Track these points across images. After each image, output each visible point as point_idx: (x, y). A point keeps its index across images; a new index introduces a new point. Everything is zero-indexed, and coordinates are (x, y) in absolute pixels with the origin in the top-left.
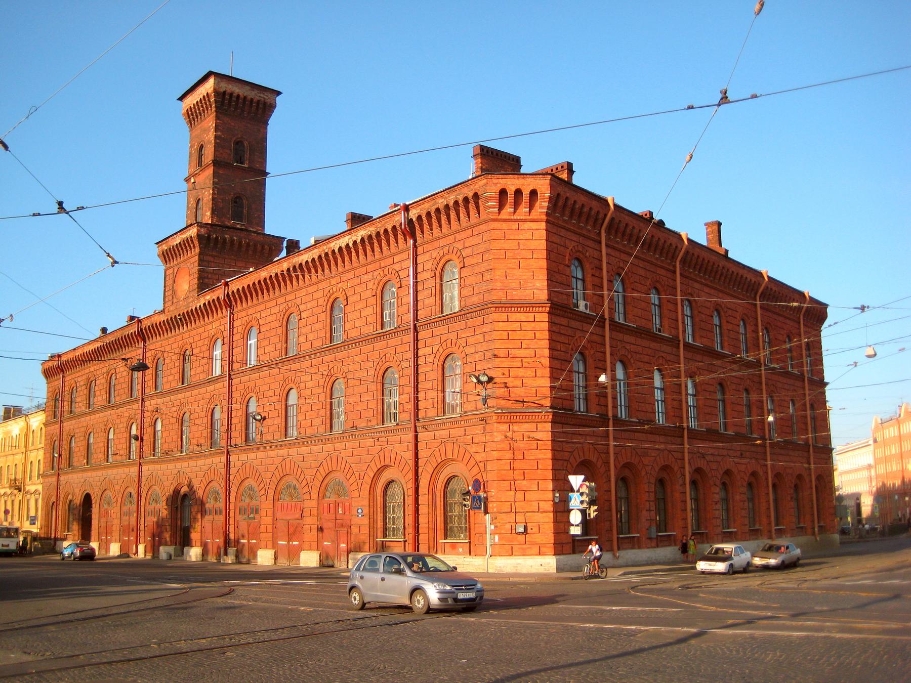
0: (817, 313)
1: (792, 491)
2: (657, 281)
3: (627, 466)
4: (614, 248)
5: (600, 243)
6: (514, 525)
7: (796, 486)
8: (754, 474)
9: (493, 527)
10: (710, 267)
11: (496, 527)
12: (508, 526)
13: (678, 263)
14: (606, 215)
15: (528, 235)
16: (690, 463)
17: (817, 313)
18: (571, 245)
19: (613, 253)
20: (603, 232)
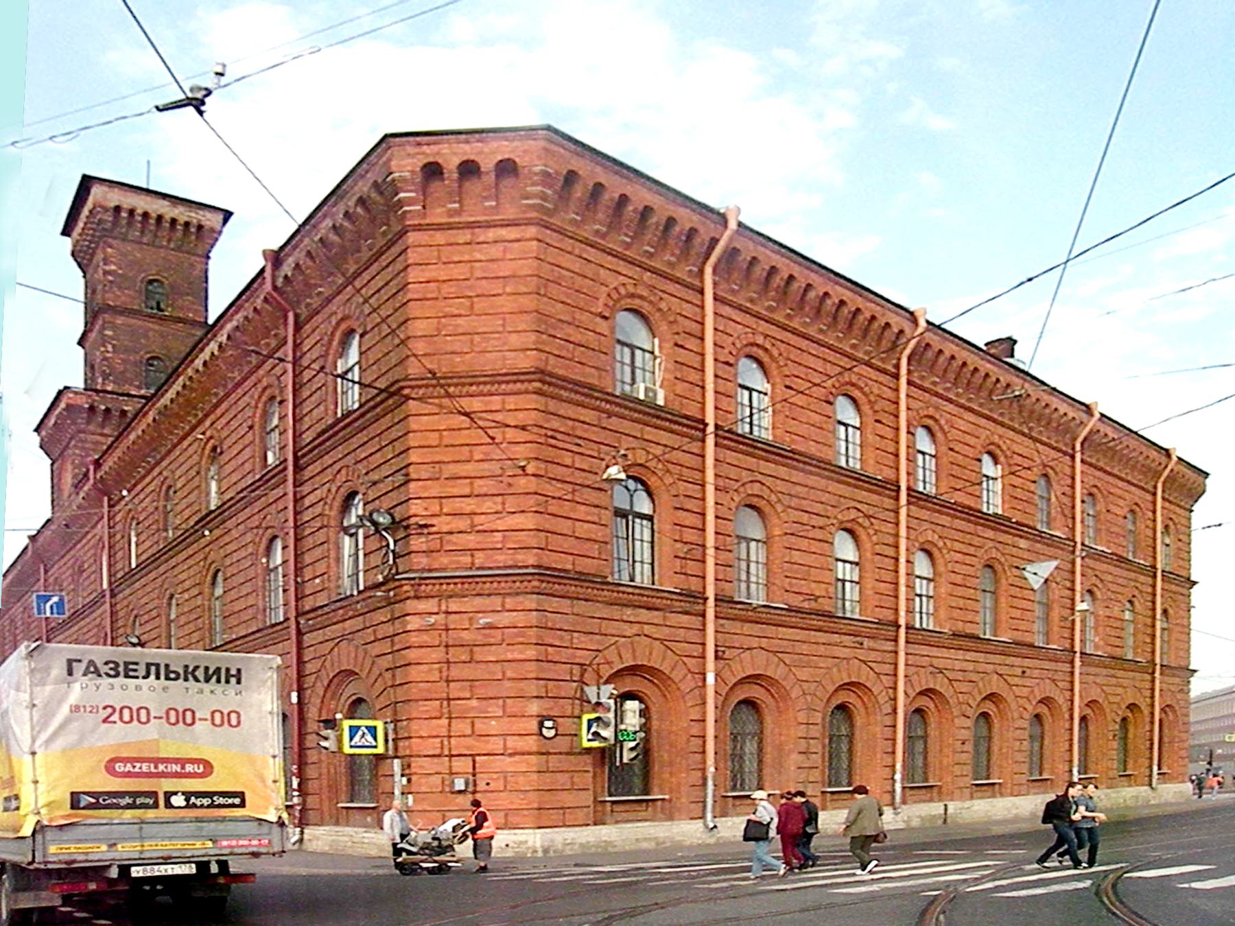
0: (1187, 484)
1: (1117, 727)
2: (992, 444)
3: (1091, 704)
4: (1090, 465)
5: (702, 292)
6: (471, 778)
7: (1124, 719)
8: (1132, 707)
9: (404, 780)
10: (983, 382)
11: (409, 781)
12: (437, 780)
13: (1160, 486)
14: (714, 242)
15: (495, 251)
16: (1081, 696)
17: (1187, 484)
18: (984, 434)
19: (1167, 505)
20: (708, 270)
